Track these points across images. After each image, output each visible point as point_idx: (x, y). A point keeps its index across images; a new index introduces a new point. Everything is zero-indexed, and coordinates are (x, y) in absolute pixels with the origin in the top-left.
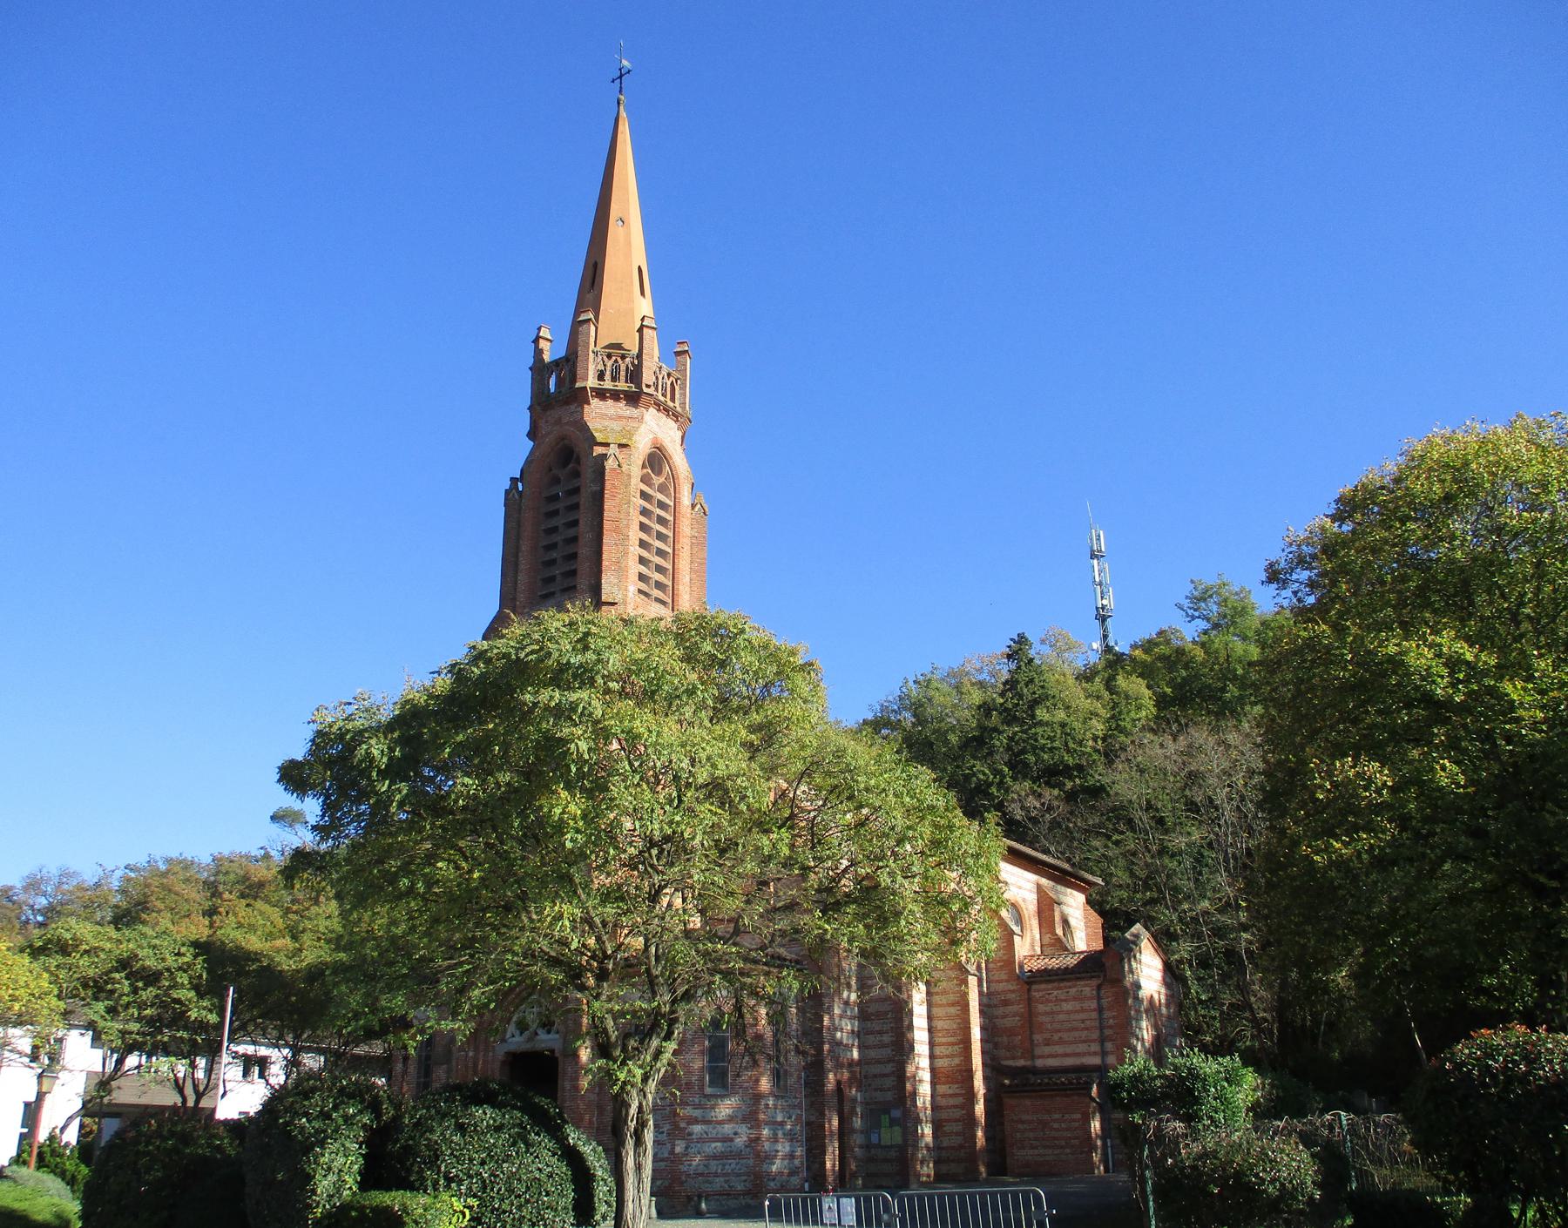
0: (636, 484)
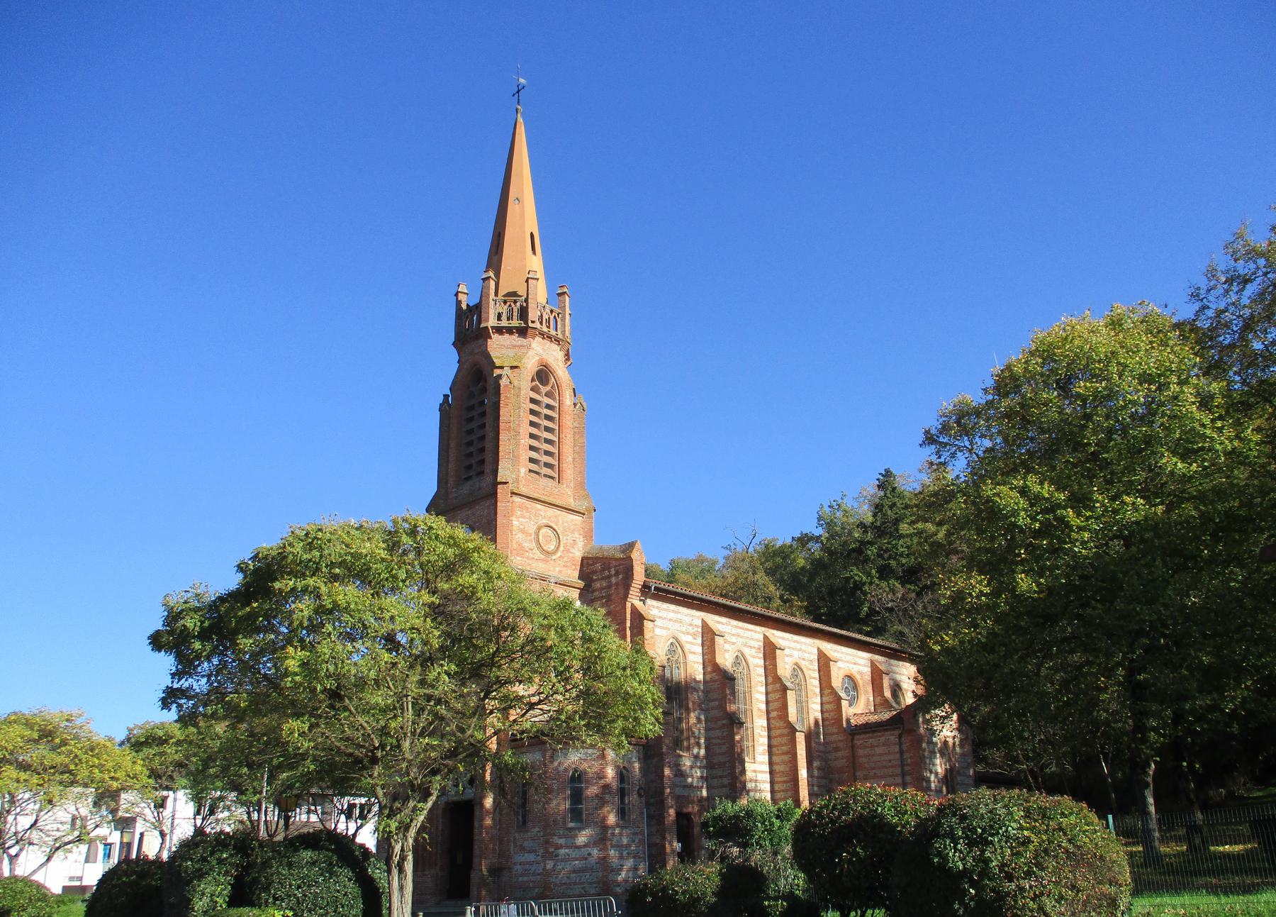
0: (527, 393)
